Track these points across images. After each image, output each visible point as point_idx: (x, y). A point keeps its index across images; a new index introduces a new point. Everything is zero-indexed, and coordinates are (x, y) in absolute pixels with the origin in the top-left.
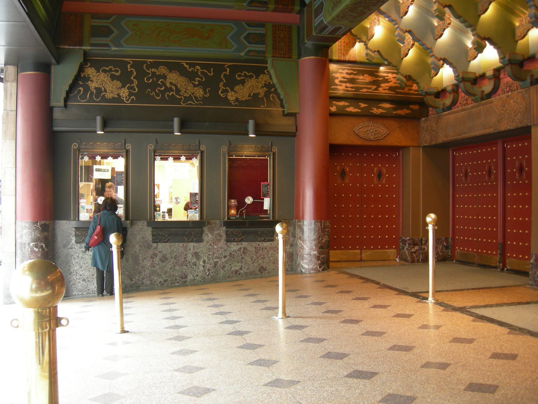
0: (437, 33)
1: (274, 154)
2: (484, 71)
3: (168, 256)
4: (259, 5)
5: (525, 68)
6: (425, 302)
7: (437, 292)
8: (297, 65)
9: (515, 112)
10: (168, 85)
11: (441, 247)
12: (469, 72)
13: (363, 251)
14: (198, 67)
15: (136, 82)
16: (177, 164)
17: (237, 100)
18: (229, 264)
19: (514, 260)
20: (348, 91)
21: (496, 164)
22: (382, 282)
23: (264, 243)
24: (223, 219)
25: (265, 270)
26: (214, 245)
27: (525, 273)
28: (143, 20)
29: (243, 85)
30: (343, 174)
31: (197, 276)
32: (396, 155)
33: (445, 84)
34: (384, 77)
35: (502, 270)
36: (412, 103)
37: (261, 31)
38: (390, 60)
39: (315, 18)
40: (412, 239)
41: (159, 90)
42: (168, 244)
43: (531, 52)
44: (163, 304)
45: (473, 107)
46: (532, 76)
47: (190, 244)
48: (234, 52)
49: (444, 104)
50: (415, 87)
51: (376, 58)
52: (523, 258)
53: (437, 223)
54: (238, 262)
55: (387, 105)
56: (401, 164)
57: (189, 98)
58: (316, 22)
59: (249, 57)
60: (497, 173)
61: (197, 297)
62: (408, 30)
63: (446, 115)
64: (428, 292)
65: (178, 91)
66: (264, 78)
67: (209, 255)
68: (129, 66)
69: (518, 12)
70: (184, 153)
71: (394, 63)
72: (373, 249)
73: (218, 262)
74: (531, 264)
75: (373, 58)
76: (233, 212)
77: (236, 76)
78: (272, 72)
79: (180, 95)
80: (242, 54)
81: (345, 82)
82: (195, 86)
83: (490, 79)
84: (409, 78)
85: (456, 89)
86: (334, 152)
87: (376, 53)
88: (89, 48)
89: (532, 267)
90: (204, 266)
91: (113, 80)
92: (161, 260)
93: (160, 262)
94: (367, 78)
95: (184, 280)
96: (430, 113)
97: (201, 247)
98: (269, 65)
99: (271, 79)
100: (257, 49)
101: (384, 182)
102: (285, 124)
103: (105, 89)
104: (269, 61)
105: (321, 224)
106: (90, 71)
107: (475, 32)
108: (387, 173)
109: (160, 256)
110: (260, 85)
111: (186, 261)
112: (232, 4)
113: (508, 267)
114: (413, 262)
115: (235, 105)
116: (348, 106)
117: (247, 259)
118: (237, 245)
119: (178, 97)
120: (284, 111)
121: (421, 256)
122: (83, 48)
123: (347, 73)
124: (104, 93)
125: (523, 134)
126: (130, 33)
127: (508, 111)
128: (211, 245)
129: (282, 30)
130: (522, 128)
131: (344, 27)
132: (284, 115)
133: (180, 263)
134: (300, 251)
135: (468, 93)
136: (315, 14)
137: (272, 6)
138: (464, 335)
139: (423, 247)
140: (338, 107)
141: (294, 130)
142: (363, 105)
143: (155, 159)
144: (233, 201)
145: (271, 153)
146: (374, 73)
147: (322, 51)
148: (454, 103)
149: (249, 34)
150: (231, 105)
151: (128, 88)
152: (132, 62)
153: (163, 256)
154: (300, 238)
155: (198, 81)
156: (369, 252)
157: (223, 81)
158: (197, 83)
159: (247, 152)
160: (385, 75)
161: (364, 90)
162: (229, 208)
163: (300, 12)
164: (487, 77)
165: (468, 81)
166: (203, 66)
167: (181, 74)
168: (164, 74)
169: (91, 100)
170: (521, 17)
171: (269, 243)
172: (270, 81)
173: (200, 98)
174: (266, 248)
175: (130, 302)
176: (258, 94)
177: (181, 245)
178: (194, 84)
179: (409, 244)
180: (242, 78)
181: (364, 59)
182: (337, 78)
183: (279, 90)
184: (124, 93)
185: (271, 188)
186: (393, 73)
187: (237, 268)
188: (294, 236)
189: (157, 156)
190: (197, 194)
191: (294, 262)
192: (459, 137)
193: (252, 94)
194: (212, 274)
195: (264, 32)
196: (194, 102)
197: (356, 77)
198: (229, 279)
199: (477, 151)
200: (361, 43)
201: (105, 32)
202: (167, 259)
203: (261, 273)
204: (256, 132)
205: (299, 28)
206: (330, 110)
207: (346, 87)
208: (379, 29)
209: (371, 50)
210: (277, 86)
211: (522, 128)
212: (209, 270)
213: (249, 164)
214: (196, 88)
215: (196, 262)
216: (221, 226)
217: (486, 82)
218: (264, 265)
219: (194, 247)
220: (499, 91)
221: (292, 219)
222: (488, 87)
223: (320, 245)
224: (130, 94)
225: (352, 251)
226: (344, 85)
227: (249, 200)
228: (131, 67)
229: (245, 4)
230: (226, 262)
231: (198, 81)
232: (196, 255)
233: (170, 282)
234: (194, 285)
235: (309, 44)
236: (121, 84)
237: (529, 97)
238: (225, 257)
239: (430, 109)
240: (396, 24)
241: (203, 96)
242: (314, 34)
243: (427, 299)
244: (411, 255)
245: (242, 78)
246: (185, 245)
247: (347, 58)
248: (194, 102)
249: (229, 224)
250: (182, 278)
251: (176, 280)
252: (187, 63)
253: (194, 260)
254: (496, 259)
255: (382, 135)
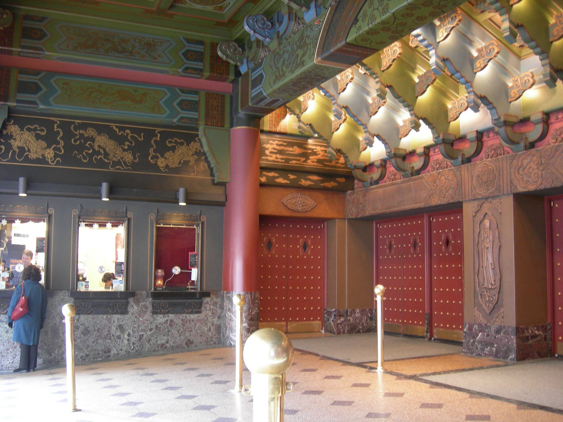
0: (371, 110)
1: (203, 223)
2: (414, 148)
3: (91, 329)
4: (194, 72)
5: (454, 147)
6: (374, 372)
7: (385, 361)
8: (229, 135)
9: (446, 188)
10: (96, 148)
11: (366, 318)
12: (400, 149)
13: (289, 323)
14: (128, 131)
15: (62, 142)
16: (103, 230)
17: (167, 166)
18: (155, 337)
19: (442, 329)
20: (278, 162)
21: (422, 235)
22: (321, 353)
23: (191, 315)
24: (150, 290)
25: (192, 343)
26: (139, 318)
27: (459, 343)
28: (74, 79)
29: (174, 152)
30: (270, 244)
31: (121, 350)
32: (321, 227)
33: (372, 159)
34: (312, 150)
35: (430, 339)
36: (340, 177)
37: (194, 98)
38: (322, 134)
39: (253, 87)
40: (338, 310)
41: (86, 153)
42: (91, 316)
43: (462, 133)
44: (99, 380)
45: (402, 183)
46: (463, 155)
47: (114, 315)
48: (167, 117)
49: (372, 178)
50: (342, 160)
51: (308, 131)
52: (451, 327)
53: (385, 294)
54: (164, 336)
55: (315, 178)
56: (326, 236)
57: (118, 163)
58: (253, 93)
59: (181, 124)
60: (423, 246)
61: (132, 372)
62: (345, 106)
63: (374, 189)
64: (377, 362)
65: (106, 155)
66: (194, 146)
67: (135, 327)
68: (55, 125)
69: (449, 95)
70: (110, 220)
71: (325, 137)
72: (298, 321)
73: (143, 335)
74: (465, 332)
75: (305, 131)
76: (160, 282)
77: (167, 142)
78: (204, 140)
79: (108, 159)
80: (175, 120)
81: (276, 153)
82: (124, 150)
83: (420, 155)
84: (339, 151)
85: (384, 163)
86: (264, 222)
87: (308, 126)
88: (15, 104)
89: (465, 336)
90: (128, 340)
91: (37, 140)
92: (82, 333)
93: (82, 336)
94: (296, 150)
95: (107, 355)
96: (356, 186)
97: (126, 320)
98: (201, 133)
99: (202, 147)
100: (190, 116)
101: (273, 252)
102: (216, 194)
103: (28, 149)
104: (201, 128)
105: (251, 296)
106: (13, 129)
107: (412, 112)
108: (312, 244)
109: (82, 328)
110: (191, 153)
111: (110, 334)
112: (166, 69)
113: (436, 337)
114: (339, 333)
115: (166, 172)
116: (278, 177)
117: (174, 331)
118: (164, 317)
119: (106, 161)
120: (214, 180)
121: (347, 327)
122: (8, 104)
123: (277, 145)
124: (28, 153)
125: (455, 208)
126: (60, 92)
127: (438, 188)
128: (136, 317)
129: (215, 99)
130: (454, 203)
131: (282, 100)
132: (214, 184)
133: (103, 337)
134: (229, 324)
135: (399, 168)
136: (252, 85)
137: (207, 74)
138: (430, 401)
139: (348, 318)
140: (268, 177)
141: (224, 200)
142: (292, 177)
143: (79, 225)
144: (160, 271)
145: (200, 222)
146: (303, 145)
147: (254, 120)
148: (382, 177)
149: (182, 100)
150: (160, 171)
151: (54, 149)
152: (59, 122)
153: (85, 329)
154: (229, 309)
155: (128, 146)
156: (294, 324)
157: (153, 147)
158: (126, 147)
159: (175, 221)
160: (314, 147)
161: (294, 162)
162: (156, 278)
163: (234, 82)
164: (417, 154)
165: (400, 157)
166: (133, 130)
167: (111, 138)
168: (92, 136)
169: (13, 159)
170: (453, 100)
171: (197, 315)
172: (200, 149)
173: (129, 163)
174: (193, 321)
175: (59, 378)
176: (189, 161)
177: (105, 317)
178: (123, 148)
179: (335, 316)
180: (173, 144)
181: (296, 131)
182: (268, 149)
183: (210, 159)
184: (49, 154)
185: (200, 259)
186: (321, 146)
187: (163, 342)
188: (222, 308)
189: (81, 222)
190: (122, 263)
191: (222, 335)
192: (388, 211)
193: (182, 161)
194: (137, 348)
195: (197, 99)
196: (123, 167)
197: (287, 148)
198: (155, 353)
199: (407, 223)
200: (292, 115)
201: (34, 89)
202: (89, 332)
203: (188, 346)
204: (187, 201)
205: (231, 97)
206: (260, 181)
207: (276, 158)
208: (312, 103)
209: (303, 123)
210: (208, 154)
211: (453, 203)
212: (134, 344)
213: (177, 233)
214: (125, 153)
215: (120, 336)
216: (147, 296)
217: (415, 158)
218: (191, 338)
219: (118, 319)
220: (429, 168)
221: (228, 288)
222: (417, 163)
223: (250, 317)
224: (56, 156)
225: (306, 322)
226: (274, 156)
227: (176, 270)
228: (58, 127)
229: (180, 70)
230: (152, 335)
231: (128, 146)
232: (121, 328)
233: (93, 357)
234: (118, 360)
235: (242, 114)
236: (46, 144)
237: (461, 174)
238: (151, 330)
239: (356, 181)
240: (334, 99)
241: (132, 161)
242: (250, 104)
243: (376, 369)
244: (337, 326)
245: (173, 144)
246: (109, 316)
247: (278, 129)
248: (123, 167)
249: (156, 295)
250: (105, 352)
251: (99, 354)
252: (116, 127)
253: (118, 333)
254: (421, 329)
255: (310, 207)
